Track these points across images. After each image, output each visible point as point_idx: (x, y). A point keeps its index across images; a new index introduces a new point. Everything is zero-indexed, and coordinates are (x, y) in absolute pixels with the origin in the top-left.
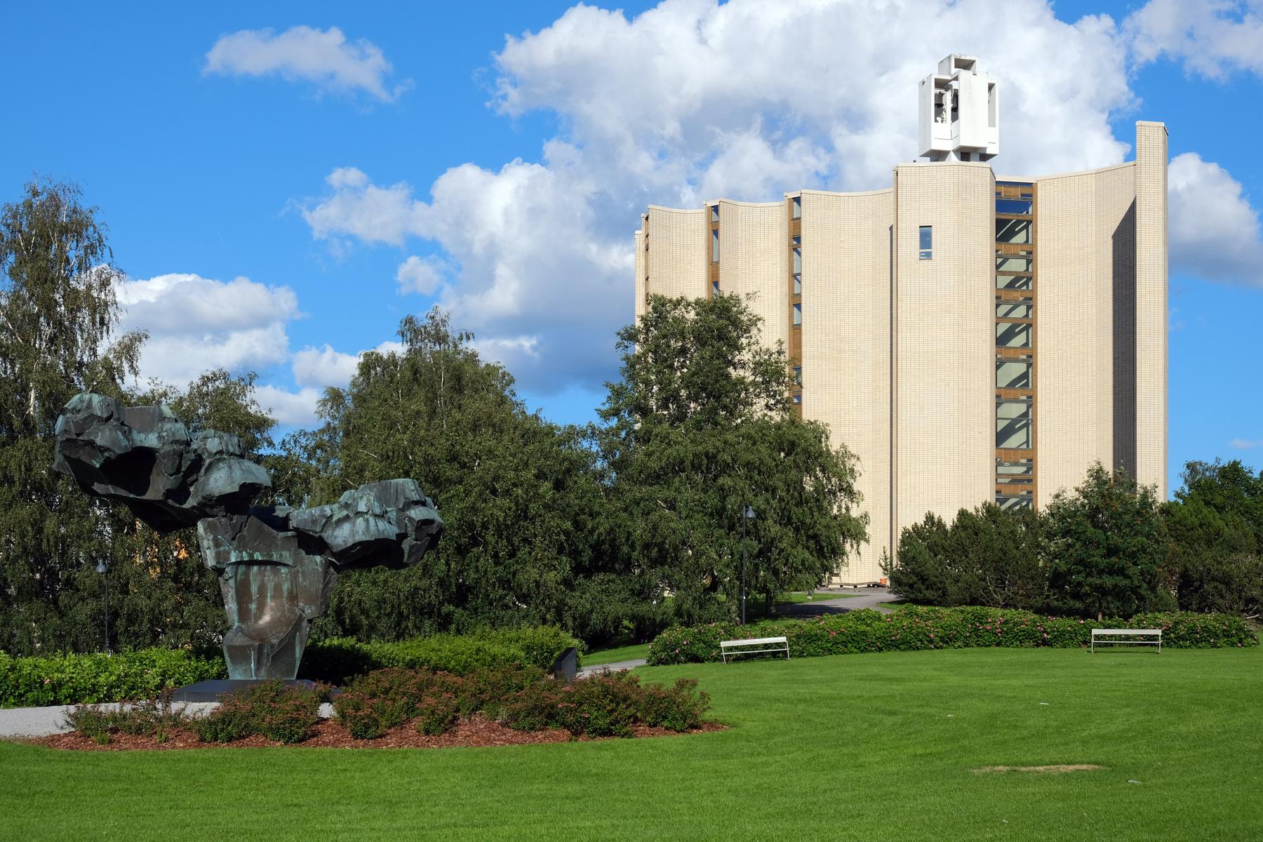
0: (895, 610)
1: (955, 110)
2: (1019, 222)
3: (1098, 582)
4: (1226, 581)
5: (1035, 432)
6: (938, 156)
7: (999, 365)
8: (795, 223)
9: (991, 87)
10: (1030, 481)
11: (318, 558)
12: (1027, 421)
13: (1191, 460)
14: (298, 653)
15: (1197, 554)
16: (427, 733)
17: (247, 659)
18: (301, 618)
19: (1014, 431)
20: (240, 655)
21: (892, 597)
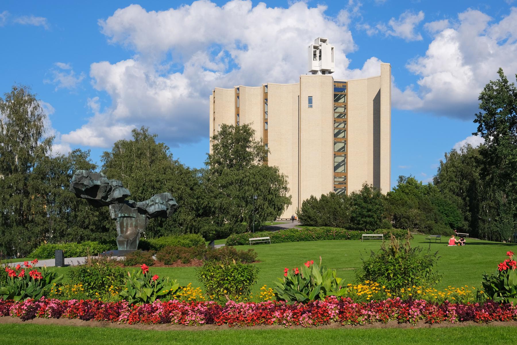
0: (300, 229)
1: (320, 56)
2: (341, 95)
3: (365, 220)
4: (408, 218)
5: (347, 167)
6: (314, 72)
7: (335, 143)
8: (266, 94)
9: (332, 49)
10: (345, 183)
11: (144, 216)
12: (344, 163)
13: (401, 175)
14: (138, 242)
15: (399, 209)
16: (184, 263)
17: (123, 244)
18: (138, 233)
19: (340, 166)
20: (122, 243)
21: (300, 224)
